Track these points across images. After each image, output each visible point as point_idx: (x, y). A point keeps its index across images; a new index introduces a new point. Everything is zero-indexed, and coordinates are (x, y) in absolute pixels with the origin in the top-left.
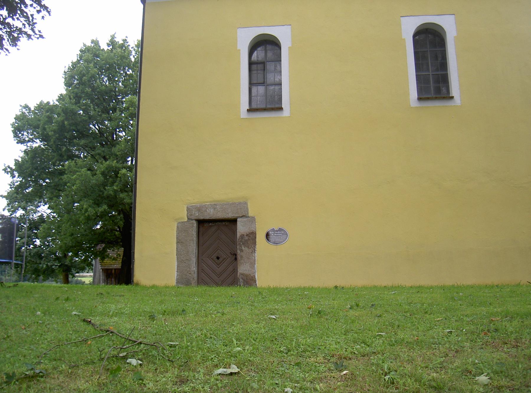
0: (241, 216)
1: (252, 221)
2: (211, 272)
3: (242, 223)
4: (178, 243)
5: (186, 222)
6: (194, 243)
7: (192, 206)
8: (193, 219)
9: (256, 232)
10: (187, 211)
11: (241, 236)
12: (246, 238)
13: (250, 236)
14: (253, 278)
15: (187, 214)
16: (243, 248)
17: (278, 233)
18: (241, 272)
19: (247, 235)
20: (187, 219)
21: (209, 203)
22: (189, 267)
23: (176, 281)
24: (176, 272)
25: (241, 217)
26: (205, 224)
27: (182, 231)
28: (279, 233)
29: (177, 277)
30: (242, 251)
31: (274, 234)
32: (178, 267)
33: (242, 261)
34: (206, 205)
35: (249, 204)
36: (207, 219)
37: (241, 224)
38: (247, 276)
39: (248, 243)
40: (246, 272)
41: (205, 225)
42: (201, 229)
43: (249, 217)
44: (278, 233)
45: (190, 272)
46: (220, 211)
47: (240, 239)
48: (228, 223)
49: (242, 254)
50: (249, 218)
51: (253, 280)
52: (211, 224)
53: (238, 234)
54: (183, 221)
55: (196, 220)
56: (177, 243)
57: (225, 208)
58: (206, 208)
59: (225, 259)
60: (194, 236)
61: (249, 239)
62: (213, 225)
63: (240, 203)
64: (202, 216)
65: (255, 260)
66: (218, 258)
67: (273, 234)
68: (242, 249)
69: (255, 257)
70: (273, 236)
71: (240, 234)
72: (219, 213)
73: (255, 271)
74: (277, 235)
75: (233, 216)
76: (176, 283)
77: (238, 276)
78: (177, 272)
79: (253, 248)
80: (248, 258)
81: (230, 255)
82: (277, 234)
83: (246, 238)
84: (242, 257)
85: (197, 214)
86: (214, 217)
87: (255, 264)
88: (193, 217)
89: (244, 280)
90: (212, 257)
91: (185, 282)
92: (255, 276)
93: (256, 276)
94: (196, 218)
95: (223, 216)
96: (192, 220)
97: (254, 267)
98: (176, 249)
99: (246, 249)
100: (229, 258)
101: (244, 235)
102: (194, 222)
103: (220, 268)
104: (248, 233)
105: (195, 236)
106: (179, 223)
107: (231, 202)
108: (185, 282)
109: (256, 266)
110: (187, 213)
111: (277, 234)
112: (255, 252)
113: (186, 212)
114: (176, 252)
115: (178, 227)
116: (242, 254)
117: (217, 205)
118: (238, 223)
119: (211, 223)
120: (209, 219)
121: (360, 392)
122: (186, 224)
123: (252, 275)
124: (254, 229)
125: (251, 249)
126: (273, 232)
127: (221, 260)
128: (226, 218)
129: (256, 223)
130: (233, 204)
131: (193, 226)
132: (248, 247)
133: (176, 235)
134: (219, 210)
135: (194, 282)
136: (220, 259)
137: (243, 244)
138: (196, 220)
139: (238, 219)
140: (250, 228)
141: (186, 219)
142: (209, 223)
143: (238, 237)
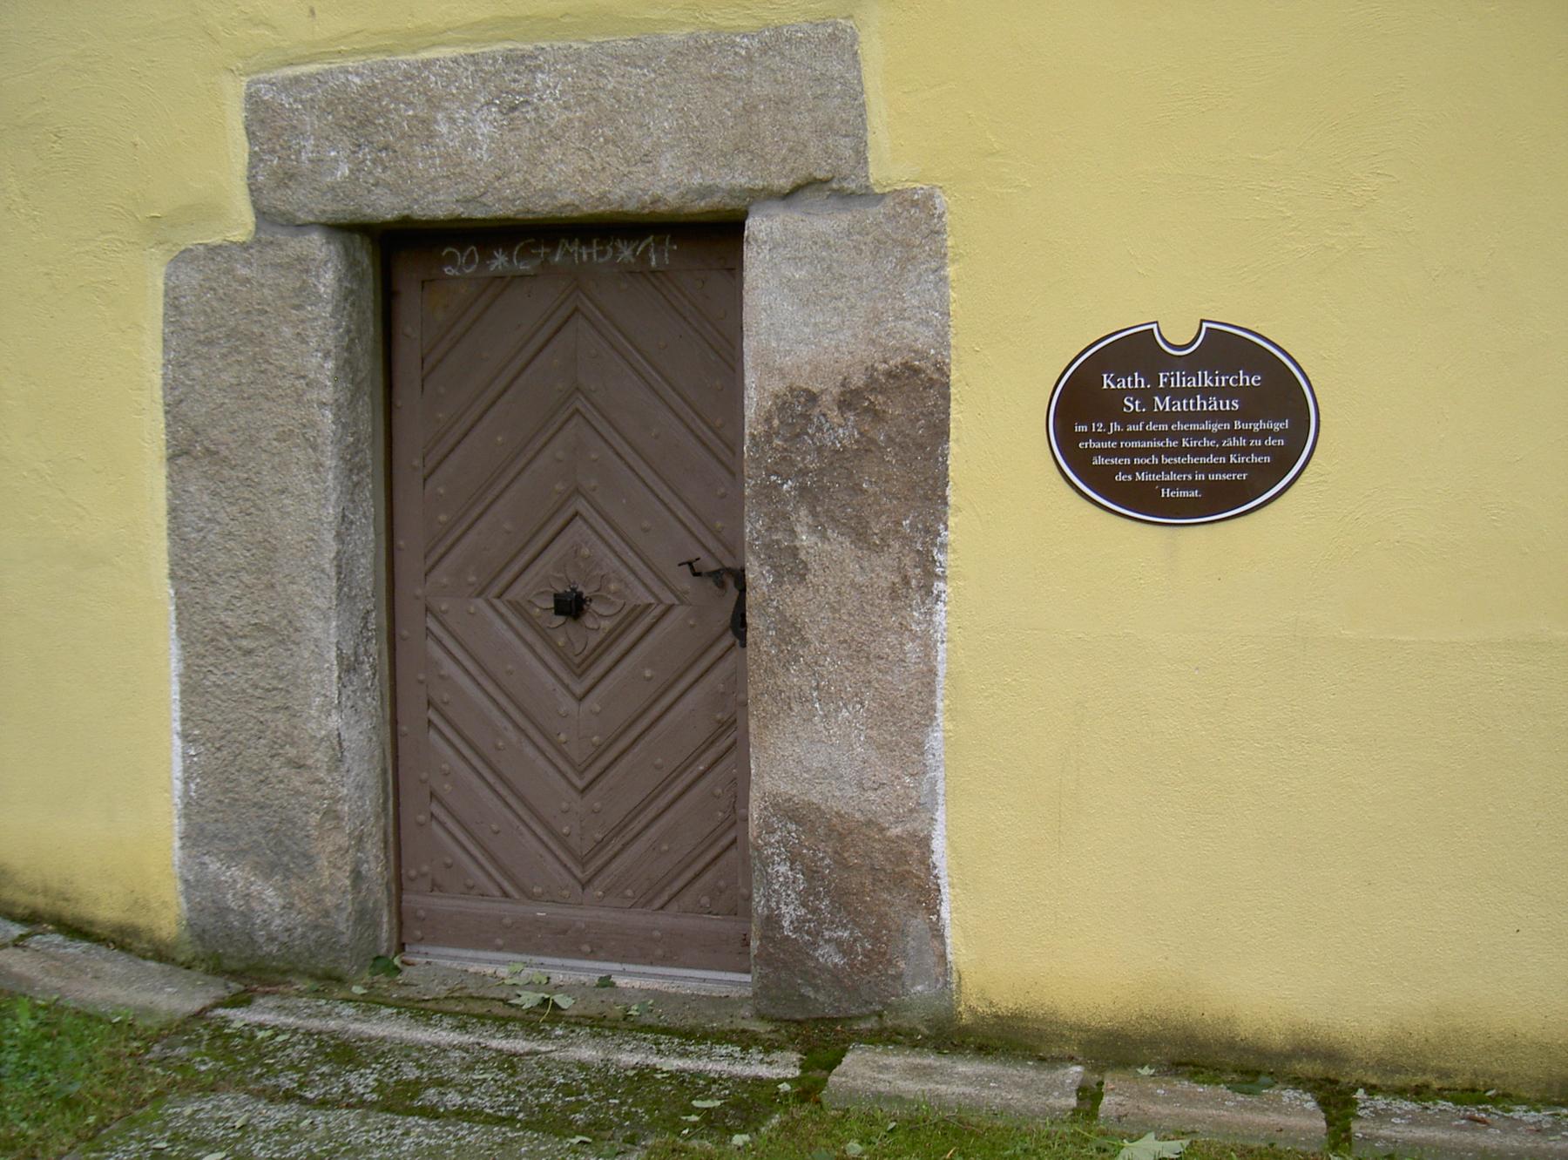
0: (784, 183)
1: (908, 246)
2: (512, 734)
3: (796, 260)
4: (178, 454)
5: (245, 247)
6: (318, 466)
7: (297, 80)
8: (303, 216)
9: (942, 369)
10: (251, 136)
11: (783, 406)
12: (842, 431)
13: (877, 416)
14: (903, 856)
15: (252, 166)
16: (805, 539)
17: (1190, 393)
18: (785, 788)
19: (849, 400)
20: (248, 218)
21: (460, 51)
22: (279, 700)
23: (176, 825)
24: (177, 742)
25: (789, 196)
26: (451, 259)
27: (210, 342)
28: (1206, 393)
29: (186, 783)
30: (791, 566)
31: (1145, 396)
32: (190, 690)
33: (794, 678)
34: (427, 64)
35: (872, 50)
36: (441, 213)
37: (788, 271)
38: (840, 832)
39: (857, 489)
40: (840, 798)
41: (449, 271)
42: (411, 305)
43: (866, 196)
44: (1190, 393)
45: (292, 752)
46: (567, 126)
47: (769, 437)
48: (670, 247)
49: (795, 600)
50: (876, 212)
51: (901, 880)
52: (499, 261)
53: (750, 379)
54: (216, 240)
55: (347, 230)
56: (171, 459)
57: (614, 94)
58: (433, 103)
59: (640, 611)
60: (313, 395)
61: (867, 447)
62: (524, 267)
63: (775, 42)
64: (393, 189)
65: (932, 672)
66: (571, 606)
67: (1136, 393)
68: (794, 552)
69: (928, 647)
70: (1134, 418)
71: (778, 386)
72: (554, 152)
73: (933, 792)
74: (1187, 417)
75: (697, 180)
76: (185, 837)
77: (753, 830)
78: (185, 736)
79: (907, 540)
80: (859, 652)
81: (685, 582)
82: (1179, 394)
83: (842, 431)
84: (789, 632)
85: (344, 170)
86: (498, 205)
87: (929, 713)
88: (309, 202)
89: (812, 874)
90: (516, 593)
91: (259, 837)
92: (925, 843)
93: (938, 844)
94: (344, 210)
95: (592, 189)
96: (302, 227)
97: (919, 746)
98: (162, 520)
99: (840, 546)
100: (679, 612)
101: (812, 398)
102: (317, 246)
103: (592, 703)
104: (858, 380)
105: (327, 395)
106: (185, 258)
107: (677, 34)
108: (259, 837)
109: (936, 739)
110: (255, 160)
111: (1179, 394)
112: (927, 590)
113: (238, 150)
114: (164, 544)
115: (173, 304)
116: (795, 600)
117: (532, 71)
118: (757, 262)
119: (508, 249)
120: (458, 220)
121: (1565, 1111)
122: (243, 272)
123: (896, 831)
124: (923, 338)
125: (886, 559)
126: (1139, 381)
127: (599, 619)
128: (631, 206)
129: (950, 271)
130: (699, 48)
131: (304, 294)
132: (860, 535)
133: (157, 380)
134: (560, 117)
135: (343, 841)
136: (588, 621)
137: (803, 490)
138: (347, 230)
139: (749, 222)
140: (876, 319)
141: (240, 224)
142: (487, 256)
143: (750, 413)
